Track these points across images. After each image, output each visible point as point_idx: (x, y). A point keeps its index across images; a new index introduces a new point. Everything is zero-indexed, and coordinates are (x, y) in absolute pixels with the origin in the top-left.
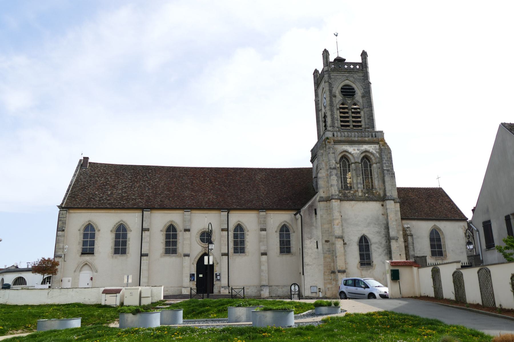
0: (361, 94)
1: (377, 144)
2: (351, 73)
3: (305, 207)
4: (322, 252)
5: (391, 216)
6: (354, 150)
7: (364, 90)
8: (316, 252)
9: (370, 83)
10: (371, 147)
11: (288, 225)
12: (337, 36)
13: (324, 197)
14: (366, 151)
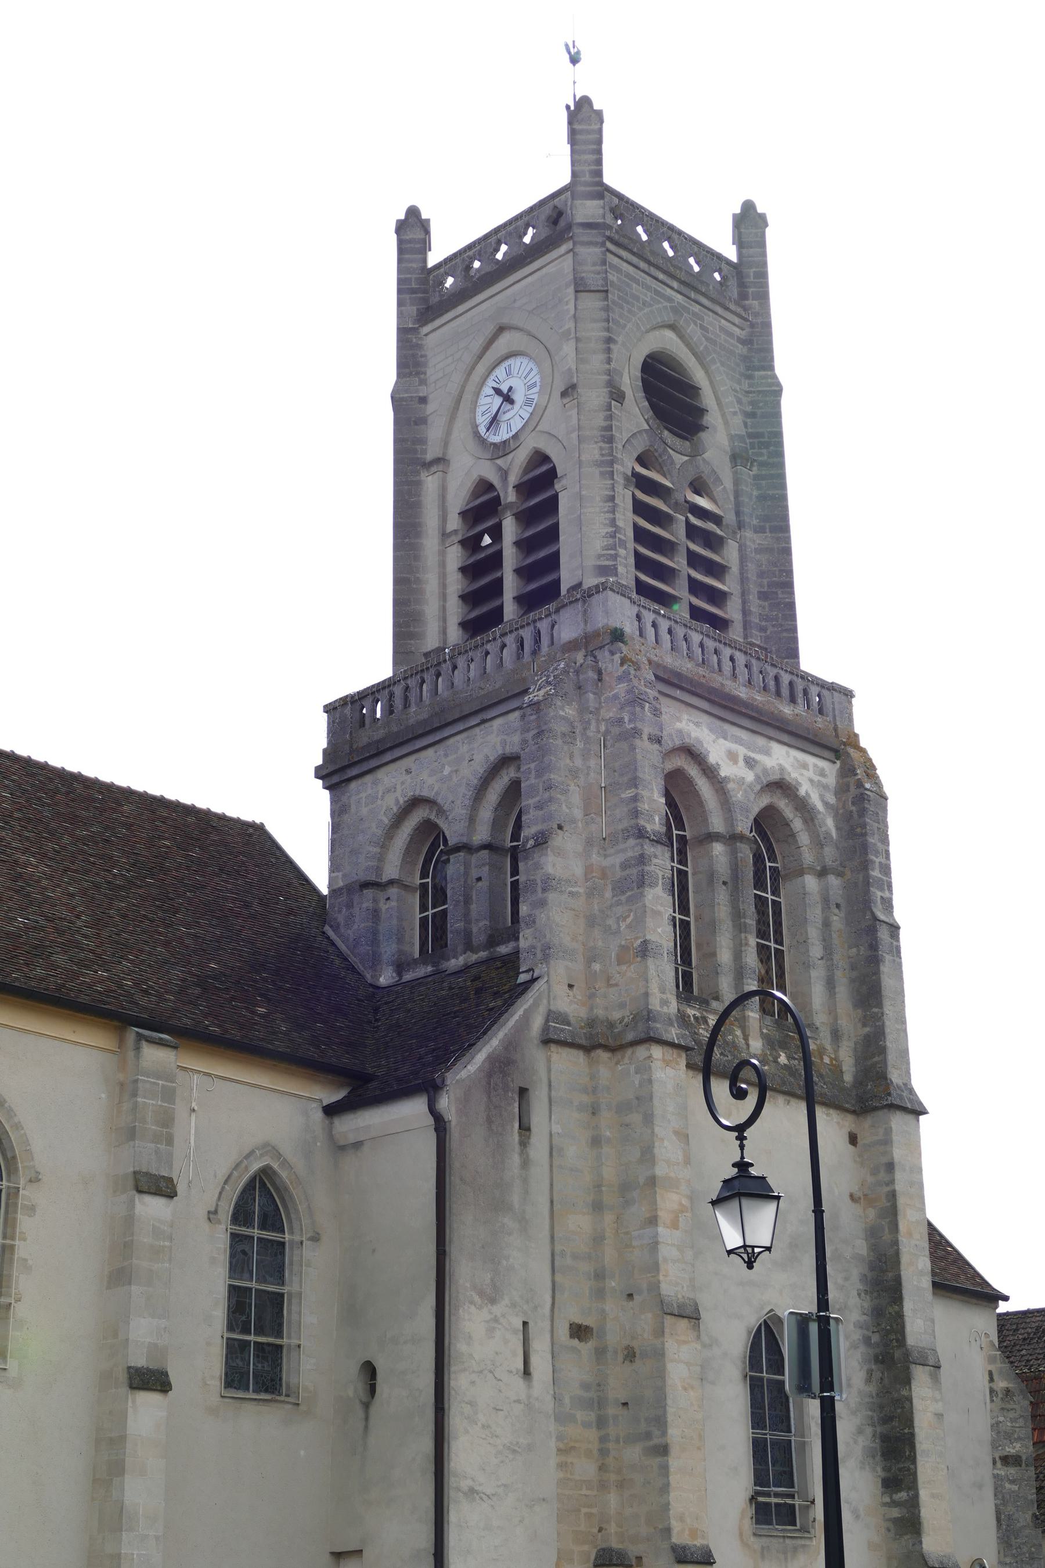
0: (732, 438)
1: (830, 755)
2: (693, 295)
3: (472, 1068)
4: (549, 1406)
5: (909, 1212)
6: (732, 757)
7: (746, 425)
8: (518, 1401)
9: (776, 391)
10: (805, 766)
11: (284, 1174)
12: (574, 60)
13: (572, 1020)
14: (781, 786)
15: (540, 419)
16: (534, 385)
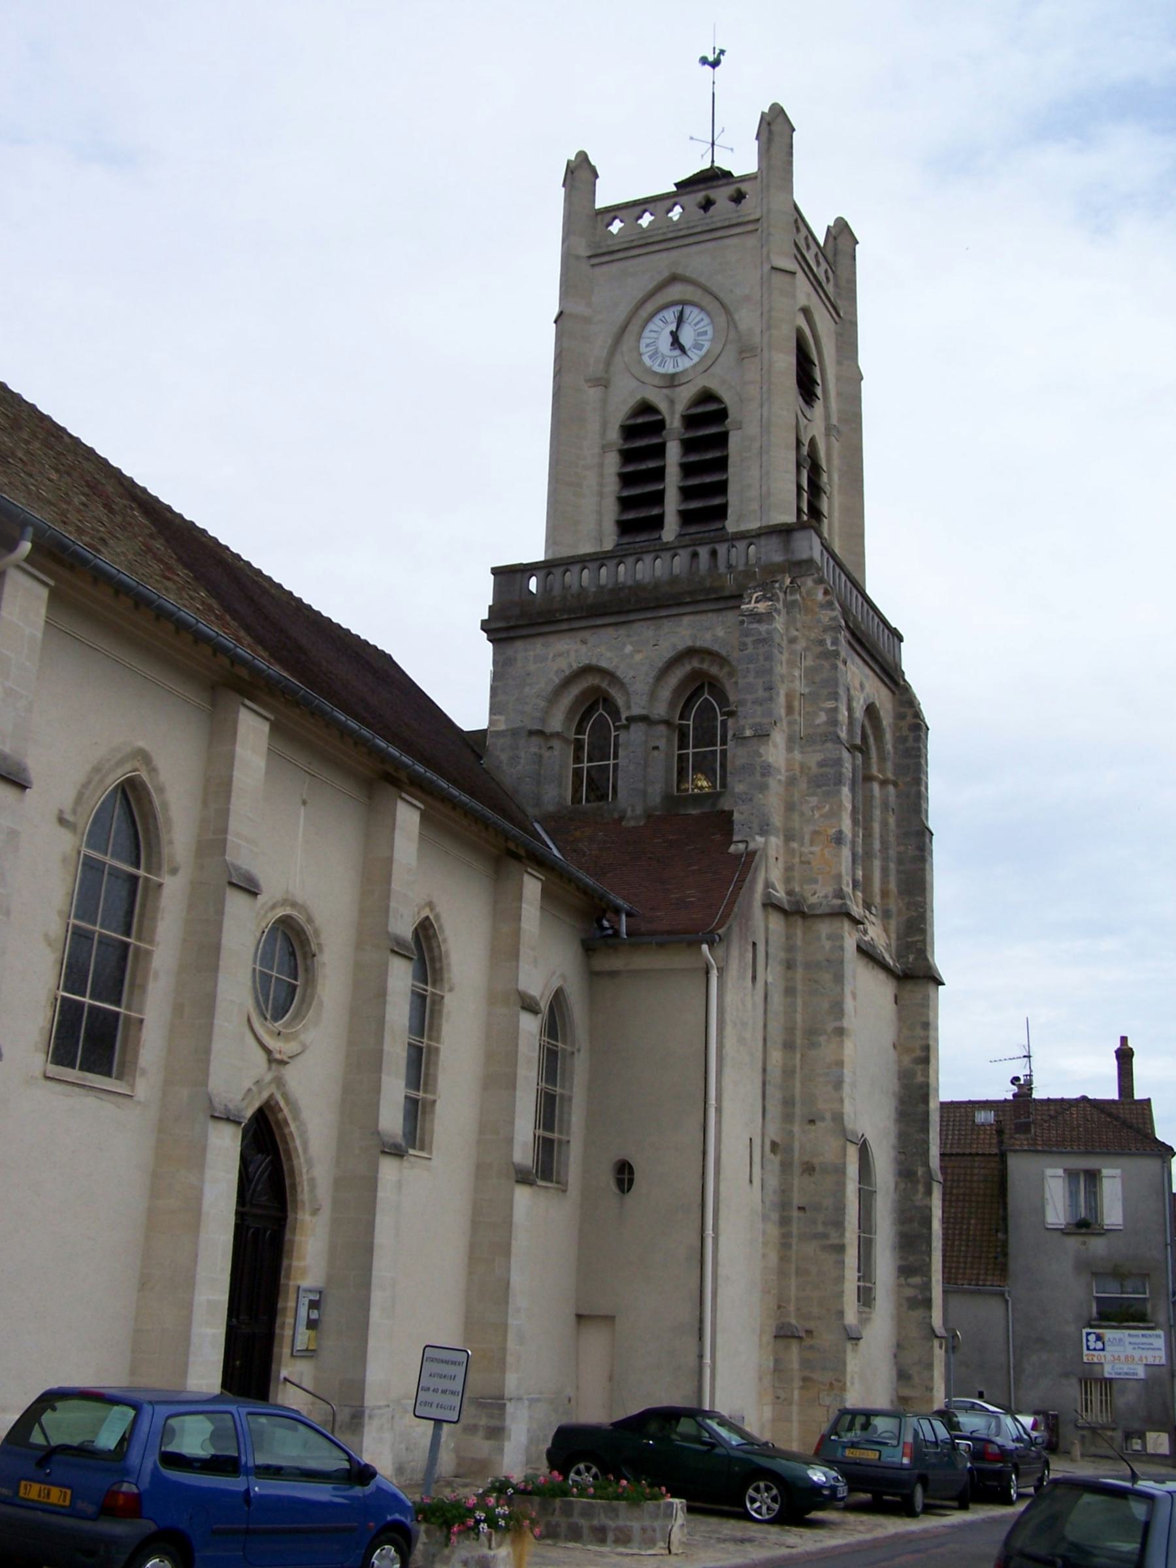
15: (713, 364)
16: (705, 333)
